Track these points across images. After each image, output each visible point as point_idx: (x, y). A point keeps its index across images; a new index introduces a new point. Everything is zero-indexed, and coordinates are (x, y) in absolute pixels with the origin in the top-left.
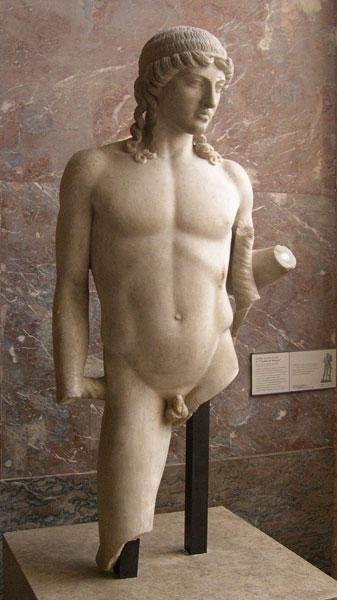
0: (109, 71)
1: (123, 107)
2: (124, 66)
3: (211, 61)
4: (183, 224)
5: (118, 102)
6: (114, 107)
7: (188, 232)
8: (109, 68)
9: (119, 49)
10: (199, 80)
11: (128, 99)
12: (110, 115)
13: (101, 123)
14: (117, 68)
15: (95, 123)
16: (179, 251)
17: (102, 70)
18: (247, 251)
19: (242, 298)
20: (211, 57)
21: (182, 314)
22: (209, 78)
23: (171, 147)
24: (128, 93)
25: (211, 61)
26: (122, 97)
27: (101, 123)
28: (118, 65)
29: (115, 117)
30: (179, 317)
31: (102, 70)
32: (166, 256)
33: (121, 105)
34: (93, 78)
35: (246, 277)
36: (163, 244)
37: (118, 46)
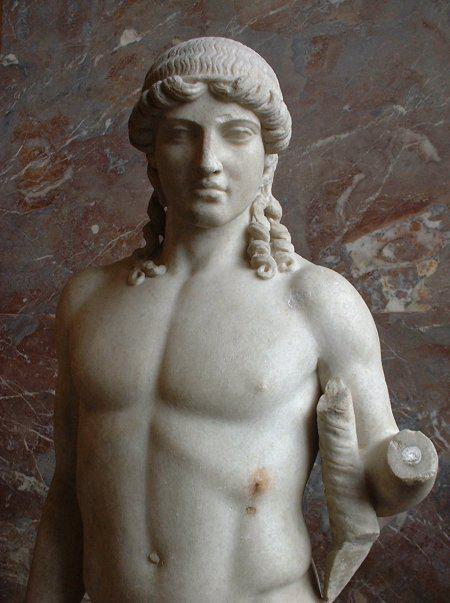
0: (330, 144)
1: (353, 192)
3: (197, 89)
5: (343, 187)
6: (338, 195)
8: (329, 139)
9: (346, 107)
12: (331, 208)
13: (317, 222)
15: (310, 221)
16: (157, 440)
17: (320, 143)
18: (340, 423)
21: (161, 554)
22: (198, 120)
23: (190, 253)
25: (197, 89)
26: (351, 179)
27: (317, 222)
28: (344, 131)
29: (340, 211)
30: (155, 557)
31: (320, 143)
32: (135, 448)
33: (349, 190)
34: (305, 157)
37: (345, 104)
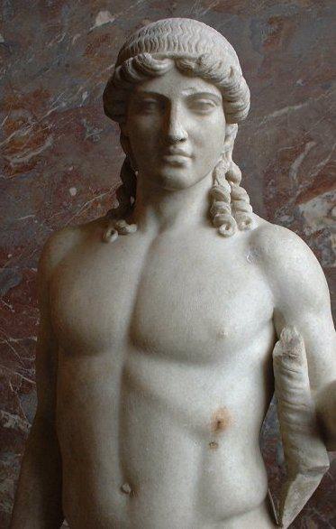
1: (304, 160)
2: (306, 104)
3: (165, 65)
4: (139, 340)
5: (297, 153)
6: (292, 160)
7: (145, 350)
9: (299, 82)
10: (151, 100)
11: (312, 148)
12: (286, 173)
14: (296, 107)
16: (129, 382)
17: (276, 114)
19: (295, 451)
20: (163, 58)
21: (132, 484)
23: (159, 213)
24: (311, 140)
25: (165, 65)
26: (303, 147)
28: (298, 103)
29: (294, 175)
30: (127, 488)
31: (276, 114)
32: (108, 388)
33: (302, 157)
34: (262, 127)
35: (294, 427)
36: (104, 374)
